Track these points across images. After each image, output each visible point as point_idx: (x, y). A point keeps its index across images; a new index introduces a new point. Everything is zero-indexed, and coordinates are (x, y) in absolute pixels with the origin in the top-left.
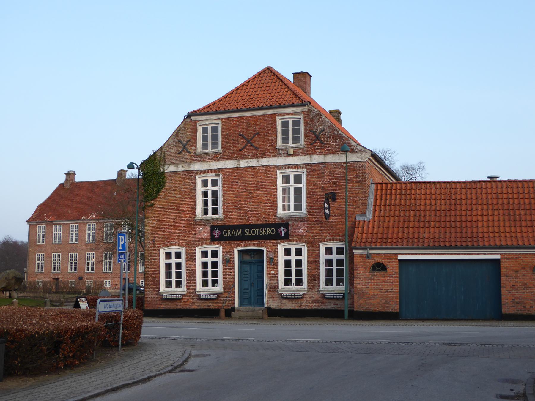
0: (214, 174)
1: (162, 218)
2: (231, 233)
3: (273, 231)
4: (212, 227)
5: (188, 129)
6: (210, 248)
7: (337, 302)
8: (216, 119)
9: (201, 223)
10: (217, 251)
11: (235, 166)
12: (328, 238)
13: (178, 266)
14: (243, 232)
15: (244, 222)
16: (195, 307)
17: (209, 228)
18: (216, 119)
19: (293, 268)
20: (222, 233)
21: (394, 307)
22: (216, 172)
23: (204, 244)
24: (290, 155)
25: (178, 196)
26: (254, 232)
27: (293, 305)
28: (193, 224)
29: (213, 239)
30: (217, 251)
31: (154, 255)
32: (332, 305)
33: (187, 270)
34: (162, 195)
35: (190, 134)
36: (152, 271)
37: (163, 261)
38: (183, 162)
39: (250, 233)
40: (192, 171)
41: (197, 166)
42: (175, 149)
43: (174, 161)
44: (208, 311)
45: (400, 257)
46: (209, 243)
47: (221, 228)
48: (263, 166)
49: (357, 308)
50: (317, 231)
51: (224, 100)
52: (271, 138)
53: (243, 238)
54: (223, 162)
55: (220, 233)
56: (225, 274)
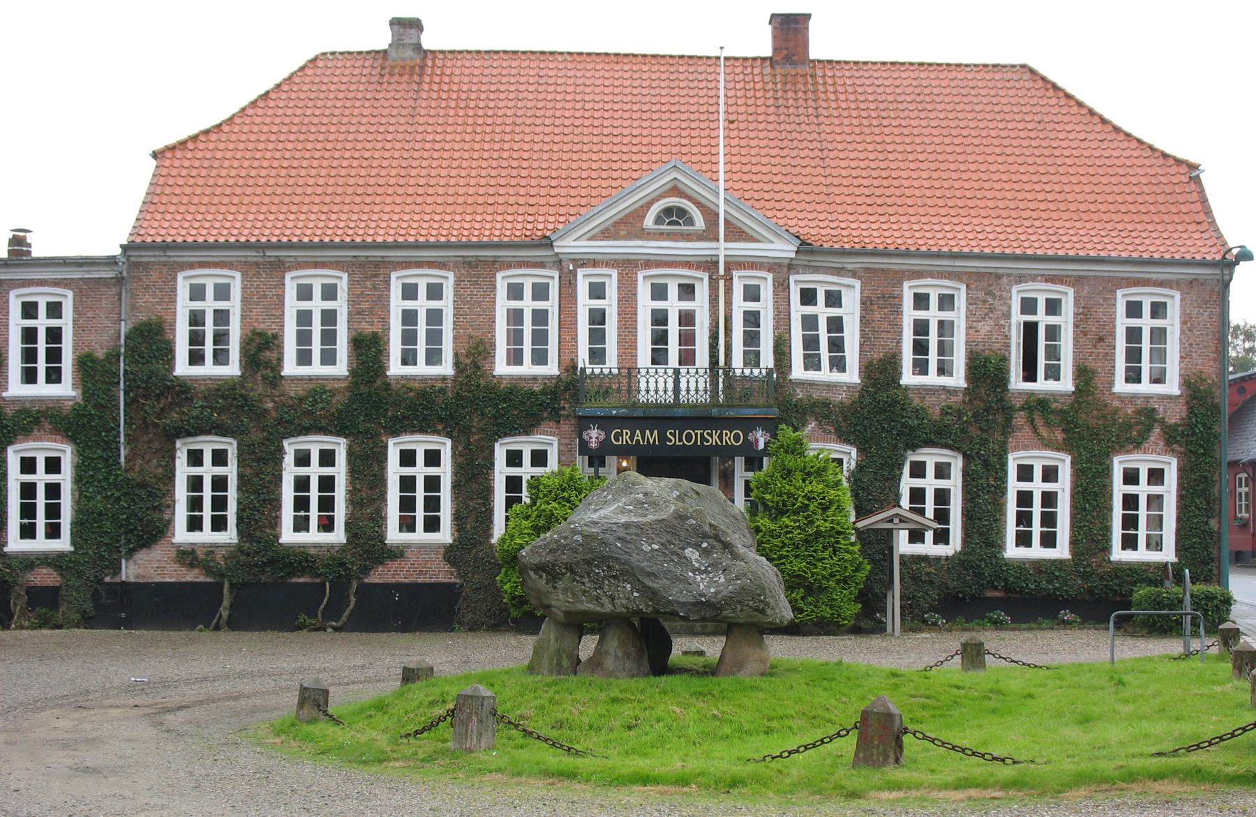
2: (632, 438)
3: (737, 438)
10: (59, 459)
19: (420, 494)
20: (608, 436)
26: (689, 438)
30: (59, 459)
39: (680, 440)
51: (226, 129)
55: (603, 436)
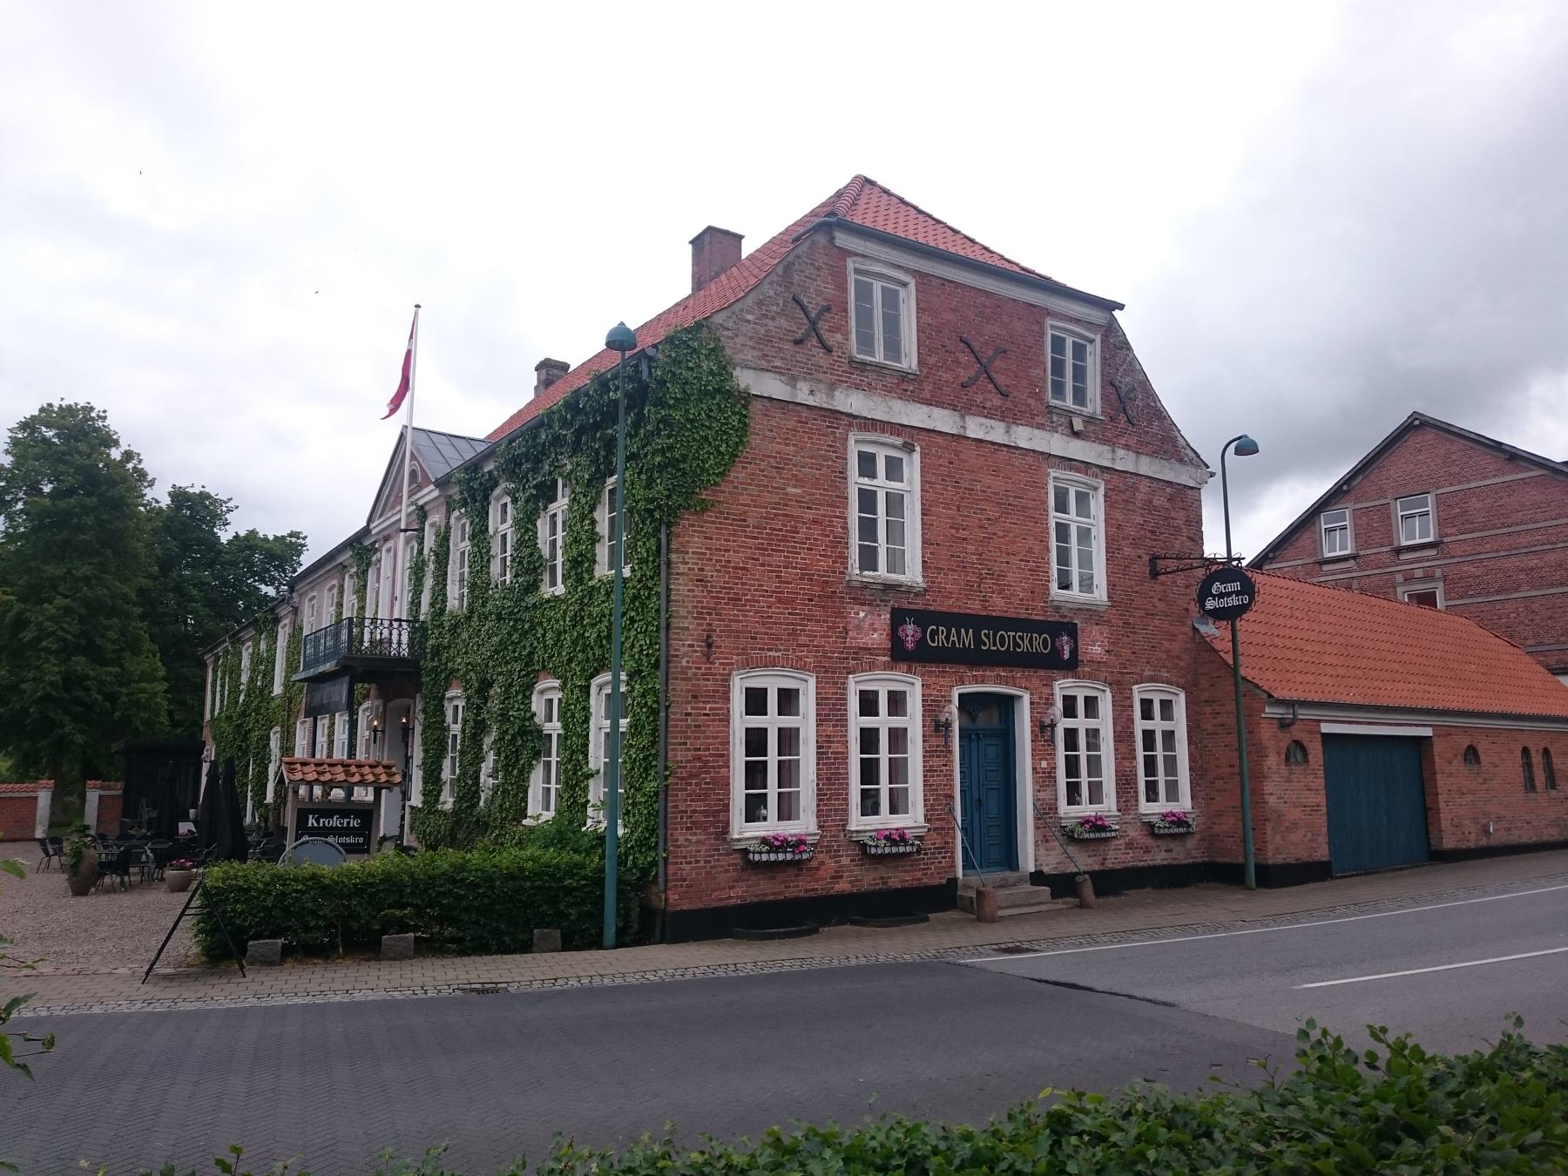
0: (899, 441)
1: (737, 559)
2: (947, 638)
4: (894, 612)
5: (819, 269)
6: (883, 683)
7: (1172, 845)
8: (899, 267)
9: (867, 594)
11: (954, 432)
12: (1147, 673)
13: (788, 739)
14: (978, 640)
15: (974, 607)
16: (843, 886)
17: (886, 616)
18: (899, 267)
21: (1322, 852)
22: (910, 436)
23: (872, 667)
24: (1077, 435)
25: (791, 490)
27: (1090, 861)
28: (835, 596)
29: (900, 655)
31: (711, 696)
32: (1163, 855)
33: (821, 755)
34: (738, 474)
35: (830, 291)
36: (699, 759)
37: (740, 722)
38: (811, 373)
40: (836, 413)
41: (853, 402)
42: (783, 322)
43: (778, 363)
44: (900, 896)
45: (1326, 728)
46: (886, 667)
47: (924, 618)
48: (1018, 448)
49: (1274, 857)
50: (1126, 652)
52: (1034, 372)
53: (974, 659)
54: (925, 409)
55: (919, 635)
56: (928, 771)
